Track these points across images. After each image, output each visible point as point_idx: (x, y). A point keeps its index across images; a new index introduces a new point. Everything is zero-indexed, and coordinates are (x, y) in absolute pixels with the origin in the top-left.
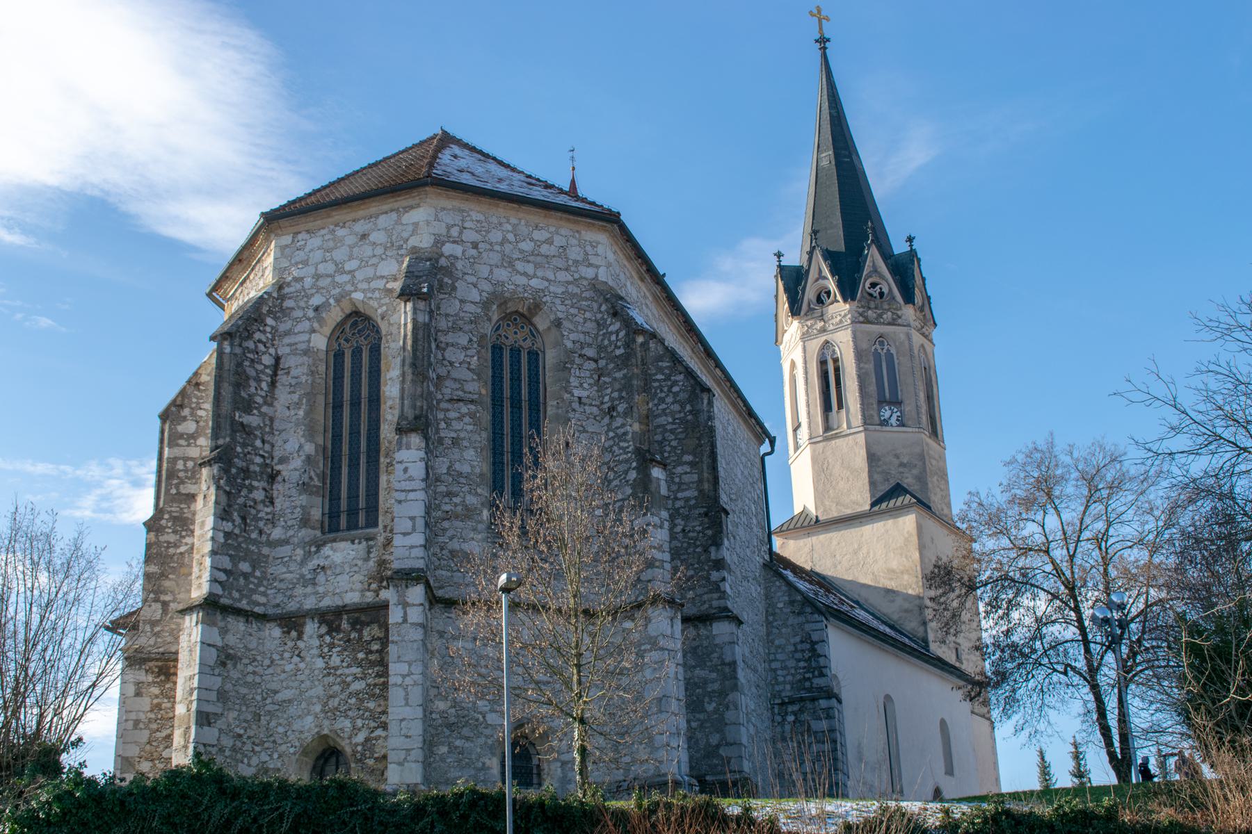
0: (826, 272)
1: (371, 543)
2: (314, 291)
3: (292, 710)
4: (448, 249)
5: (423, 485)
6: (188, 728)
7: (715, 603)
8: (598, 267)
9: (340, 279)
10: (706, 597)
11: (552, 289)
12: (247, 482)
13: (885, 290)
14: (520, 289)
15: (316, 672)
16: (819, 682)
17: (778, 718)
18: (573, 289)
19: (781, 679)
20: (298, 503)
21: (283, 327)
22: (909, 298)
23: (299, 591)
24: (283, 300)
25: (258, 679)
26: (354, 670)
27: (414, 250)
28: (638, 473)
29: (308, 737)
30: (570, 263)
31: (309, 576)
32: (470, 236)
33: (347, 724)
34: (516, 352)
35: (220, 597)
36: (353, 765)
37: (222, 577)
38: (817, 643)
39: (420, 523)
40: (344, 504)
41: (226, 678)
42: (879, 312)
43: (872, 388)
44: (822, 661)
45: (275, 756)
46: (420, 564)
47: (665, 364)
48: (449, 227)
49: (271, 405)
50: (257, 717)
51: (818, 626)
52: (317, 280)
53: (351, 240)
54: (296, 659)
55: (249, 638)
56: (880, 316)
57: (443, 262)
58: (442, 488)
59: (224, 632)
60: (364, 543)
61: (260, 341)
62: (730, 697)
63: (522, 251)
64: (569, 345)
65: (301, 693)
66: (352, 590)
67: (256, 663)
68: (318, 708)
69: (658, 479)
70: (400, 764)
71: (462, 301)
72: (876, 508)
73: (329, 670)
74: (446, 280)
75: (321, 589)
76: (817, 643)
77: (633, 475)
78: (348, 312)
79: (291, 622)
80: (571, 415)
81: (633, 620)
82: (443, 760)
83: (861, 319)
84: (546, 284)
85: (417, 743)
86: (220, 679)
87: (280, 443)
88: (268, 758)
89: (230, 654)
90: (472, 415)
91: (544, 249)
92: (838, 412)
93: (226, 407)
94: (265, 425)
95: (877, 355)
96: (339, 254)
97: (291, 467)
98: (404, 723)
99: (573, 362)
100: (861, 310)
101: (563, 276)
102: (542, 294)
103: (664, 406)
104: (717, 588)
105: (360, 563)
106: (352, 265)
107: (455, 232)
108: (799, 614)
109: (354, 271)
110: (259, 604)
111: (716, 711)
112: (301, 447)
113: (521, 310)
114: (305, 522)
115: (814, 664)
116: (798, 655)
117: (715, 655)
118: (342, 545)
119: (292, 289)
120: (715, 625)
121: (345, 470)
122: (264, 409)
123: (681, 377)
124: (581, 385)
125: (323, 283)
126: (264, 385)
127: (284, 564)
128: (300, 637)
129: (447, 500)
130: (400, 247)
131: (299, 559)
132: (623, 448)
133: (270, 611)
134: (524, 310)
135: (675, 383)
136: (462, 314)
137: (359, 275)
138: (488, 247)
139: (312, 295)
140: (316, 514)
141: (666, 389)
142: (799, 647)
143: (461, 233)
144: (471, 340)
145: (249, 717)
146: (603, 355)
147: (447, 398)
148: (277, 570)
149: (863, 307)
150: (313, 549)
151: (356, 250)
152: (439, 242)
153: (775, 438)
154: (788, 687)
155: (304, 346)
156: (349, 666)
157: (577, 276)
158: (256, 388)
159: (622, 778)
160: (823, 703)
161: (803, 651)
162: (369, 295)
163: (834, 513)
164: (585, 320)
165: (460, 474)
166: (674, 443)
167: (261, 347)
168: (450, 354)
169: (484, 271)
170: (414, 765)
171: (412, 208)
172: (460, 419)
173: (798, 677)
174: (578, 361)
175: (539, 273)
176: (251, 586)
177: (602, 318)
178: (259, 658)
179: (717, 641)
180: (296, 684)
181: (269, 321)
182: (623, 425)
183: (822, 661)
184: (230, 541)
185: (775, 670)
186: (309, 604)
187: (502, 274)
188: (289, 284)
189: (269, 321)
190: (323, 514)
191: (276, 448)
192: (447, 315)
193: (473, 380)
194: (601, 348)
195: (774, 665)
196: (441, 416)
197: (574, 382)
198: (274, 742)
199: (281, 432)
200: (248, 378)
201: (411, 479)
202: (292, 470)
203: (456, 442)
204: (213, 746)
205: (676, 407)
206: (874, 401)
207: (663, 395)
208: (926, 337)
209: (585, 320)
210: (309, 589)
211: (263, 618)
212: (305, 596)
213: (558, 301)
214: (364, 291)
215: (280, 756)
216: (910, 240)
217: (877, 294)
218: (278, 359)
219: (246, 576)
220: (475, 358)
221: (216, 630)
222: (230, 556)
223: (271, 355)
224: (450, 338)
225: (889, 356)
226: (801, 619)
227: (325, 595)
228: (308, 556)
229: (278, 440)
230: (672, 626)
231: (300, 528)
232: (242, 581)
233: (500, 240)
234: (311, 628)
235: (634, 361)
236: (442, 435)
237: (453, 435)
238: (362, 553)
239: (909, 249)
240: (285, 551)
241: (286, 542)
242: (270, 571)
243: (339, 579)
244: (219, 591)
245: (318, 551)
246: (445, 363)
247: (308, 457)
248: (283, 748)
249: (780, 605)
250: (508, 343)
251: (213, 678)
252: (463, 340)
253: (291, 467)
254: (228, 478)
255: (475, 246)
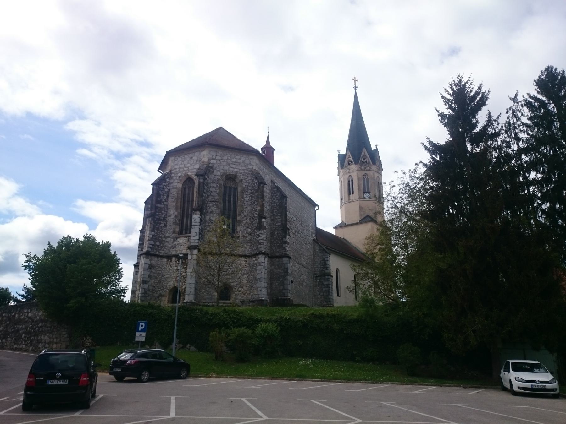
0: (351, 156)
1: (189, 238)
2: (179, 172)
3: (168, 280)
4: (212, 161)
5: (199, 224)
6: (140, 285)
7: (284, 253)
8: (253, 165)
9: (186, 169)
10: (282, 251)
11: (240, 171)
12: (159, 222)
13: (367, 161)
14: (231, 172)
15: (174, 271)
16: (326, 271)
17: (315, 281)
18: (246, 171)
19: (316, 270)
20: (172, 227)
21: (171, 181)
22: (374, 163)
23: (172, 249)
24: (171, 174)
25: (160, 272)
26: (183, 270)
27: (203, 162)
28: (259, 220)
29: (172, 287)
30: (246, 164)
31: (174, 246)
32: (218, 158)
33: (181, 283)
34: (230, 188)
35: (150, 251)
36: (181, 294)
37: (151, 246)
38: (326, 261)
39: (198, 234)
40: (184, 227)
41: (151, 272)
42: (365, 167)
43: (362, 188)
44: (327, 266)
45: (164, 291)
46: (197, 244)
47: (275, 190)
48: (212, 156)
49: (167, 202)
50: (160, 282)
51: (326, 256)
52: (180, 169)
53: (188, 159)
54: (170, 267)
55: (158, 262)
56: (365, 168)
57: (210, 165)
58: (207, 224)
59: (151, 260)
60: (187, 238)
61: (164, 185)
62: (286, 277)
63: (232, 162)
64: (244, 186)
65: (171, 275)
66: (184, 250)
67: (160, 268)
68: (174, 280)
69: (264, 222)
70: (188, 295)
71: (215, 175)
72: (360, 222)
73: (178, 270)
74: (211, 170)
75: (177, 249)
76: (326, 261)
77: (258, 220)
78: (187, 177)
79: (169, 258)
80: (244, 205)
81: (255, 258)
82: (203, 293)
83: (360, 169)
84: (239, 170)
85: (193, 289)
86: (149, 272)
87: (169, 211)
88: (162, 292)
89: (152, 266)
90: (216, 205)
91: (239, 161)
92: (352, 195)
93: (154, 202)
94: (165, 207)
95: (364, 179)
96: (186, 162)
97: (171, 218)
98: (190, 285)
99: (245, 191)
100: (360, 167)
101: (244, 168)
102: (237, 173)
103: (274, 201)
104: (284, 249)
105: (186, 243)
106: (188, 165)
107: (214, 157)
108: (322, 253)
109: (189, 167)
110: (161, 253)
111: (282, 280)
112: (174, 213)
113: (232, 177)
114: (174, 232)
115: (325, 267)
116: (321, 264)
117: (283, 266)
118: (182, 238)
119: (174, 171)
120: (283, 258)
121: (185, 219)
122: (165, 203)
123: (279, 193)
124: (247, 197)
125: (181, 170)
126: (165, 197)
127: (168, 242)
128: (171, 261)
129: (208, 227)
130: (200, 161)
131: (172, 241)
132: (256, 213)
133: (165, 255)
134: (233, 177)
135: (277, 195)
136: (215, 179)
137: (190, 168)
138: (223, 161)
139: (178, 173)
140: (177, 230)
141: (275, 196)
142: (322, 262)
143: (216, 157)
144: (217, 186)
145: (157, 282)
146: (253, 189)
147: (210, 200)
148: (166, 244)
149: (360, 166)
150: (175, 239)
151: (189, 161)
152: (209, 160)
153: (319, 206)
154: (318, 272)
155: (175, 187)
156: (182, 269)
157: (247, 168)
158: (163, 198)
159: (251, 298)
160: (327, 277)
161: (322, 263)
162: (192, 173)
163: (350, 223)
164: (249, 179)
165: (212, 220)
166: (276, 211)
167: (165, 187)
168: (211, 189)
169: (222, 167)
170: (192, 295)
171: (203, 150)
172: (213, 206)
173: (321, 270)
174: (246, 190)
175: (237, 167)
176: (160, 248)
177: (253, 179)
178: (161, 267)
179: (284, 262)
180: (169, 273)
181: (167, 180)
182: (256, 208)
183: (327, 266)
184: (153, 237)
185: (315, 268)
186: (174, 253)
187: (226, 168)
188: (173, 170)
189: (167, 180)
190: (179, 230)
191: (168, 213)
192: (211, 179)
193: (217, 196)
194: (253, 187)
195: (315, 266)
196: (208, 205)
197: (245, 196)
198: (164, 288)
199: (169, 208)
200: (160, 195)
201: (196, 222)
202: (171, 219)
203: (212, 212)
204: (147, 289)
205: (277, 201)
206: (362, 192)
207: (274, 198)
208: (379, 173)
209: (249, 179)
210: (174, 249)
211: (162, 257)
212: (173, 251)
213: (242, 175)
214: (191, 172)
215: (165, 291)
216: (376, 146)
217: (365, 162)
218: (169, 190)
219: (158, 246)
220: (218, 190)
221: (149, 260)
222: (154, 241)
223: (167, 189)
224: (212, 185)
225: (368, 179)
226: (322, 254)
227: (177, 251)
228: (174, 241)
229: (169, 211)
230: (265, 260)
231: (173, 233)
232: (157, 247)
233: (226, 159)
234: (174, 259)
235: (260, 191)
236: (208, 210)
237: (211, 210)
238: (187, 241)
239: (376, 148)
240: (169, 239)
241: (168, 237)
242: (165, 244)
243: (181, 247)
244: (150, 250)
245: (177, 239)
246: (210, 191)
247: (176, 216)
248: (166, 289)
249: (317, 250)
250: (228, 186)
251: (148, 272)
252: (215, 185)
253: (171, 218)
254: (154, 221)
255: (219, 160)
